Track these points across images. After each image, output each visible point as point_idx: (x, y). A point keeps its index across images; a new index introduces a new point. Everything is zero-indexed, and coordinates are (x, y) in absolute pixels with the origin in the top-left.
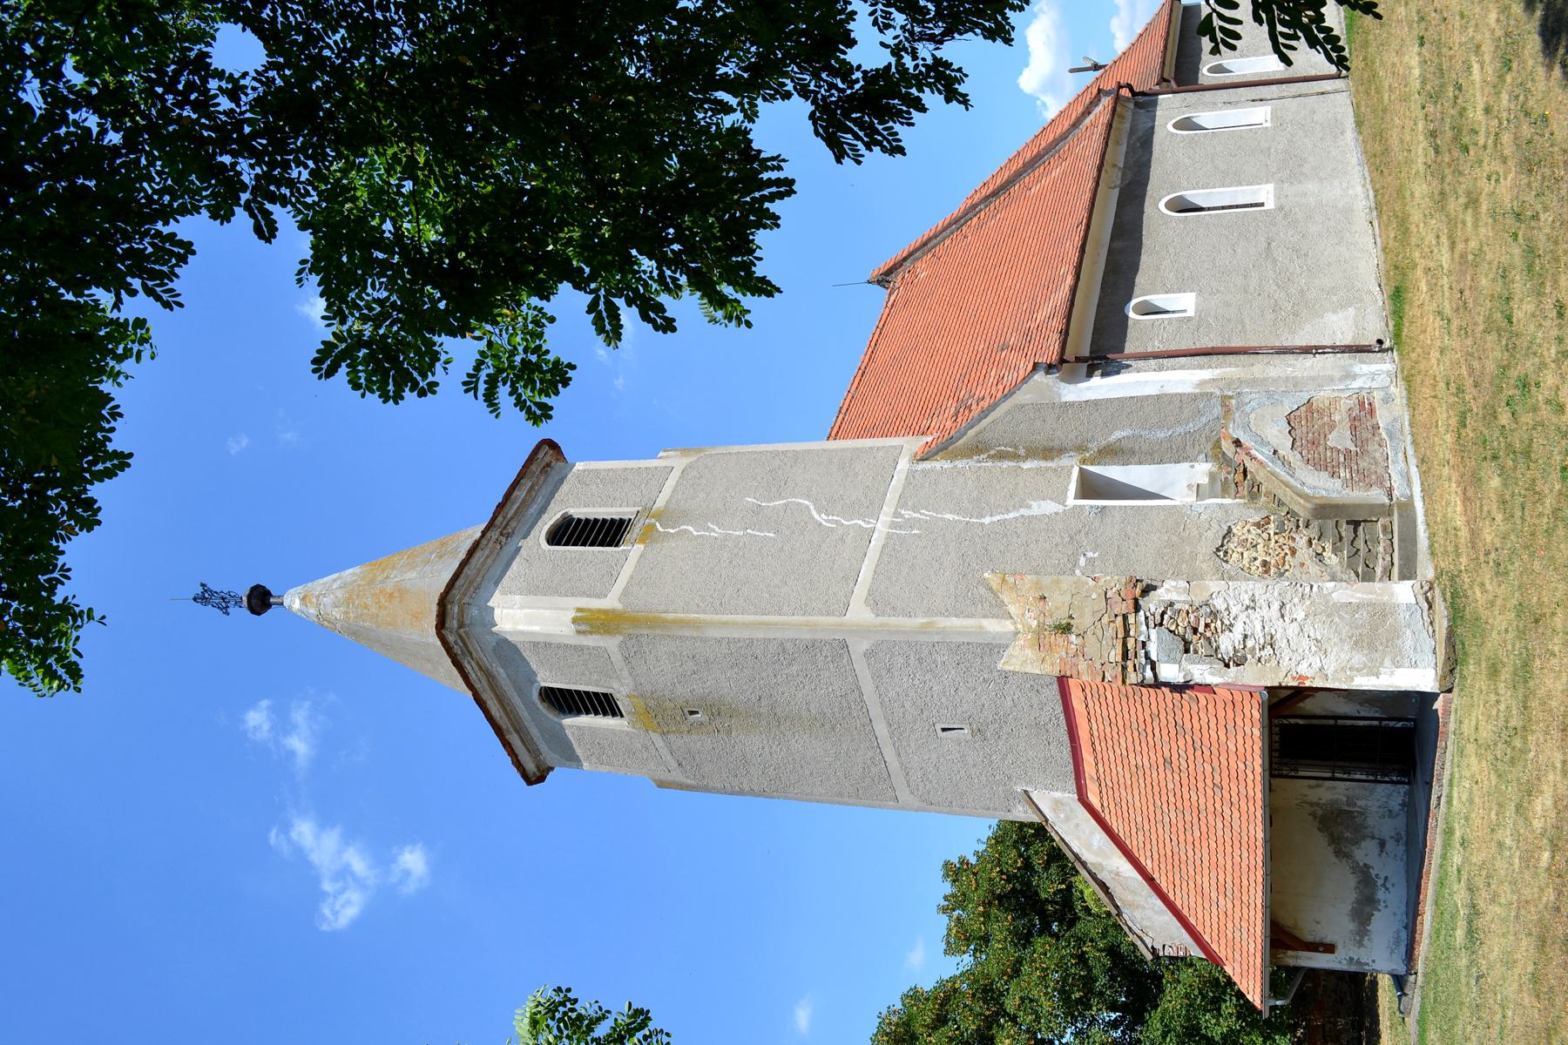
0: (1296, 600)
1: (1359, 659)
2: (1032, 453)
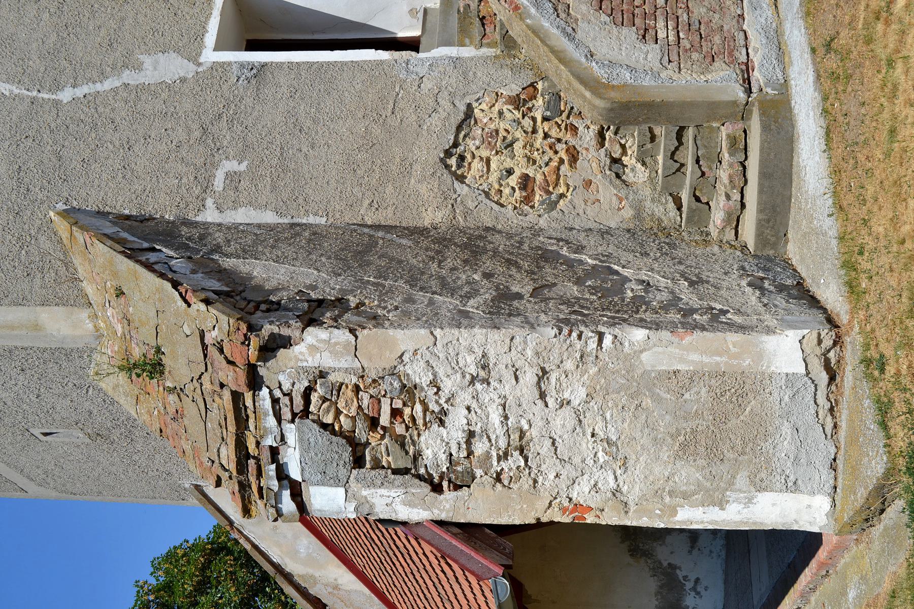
0: (569, 365)
1: (687, 474)
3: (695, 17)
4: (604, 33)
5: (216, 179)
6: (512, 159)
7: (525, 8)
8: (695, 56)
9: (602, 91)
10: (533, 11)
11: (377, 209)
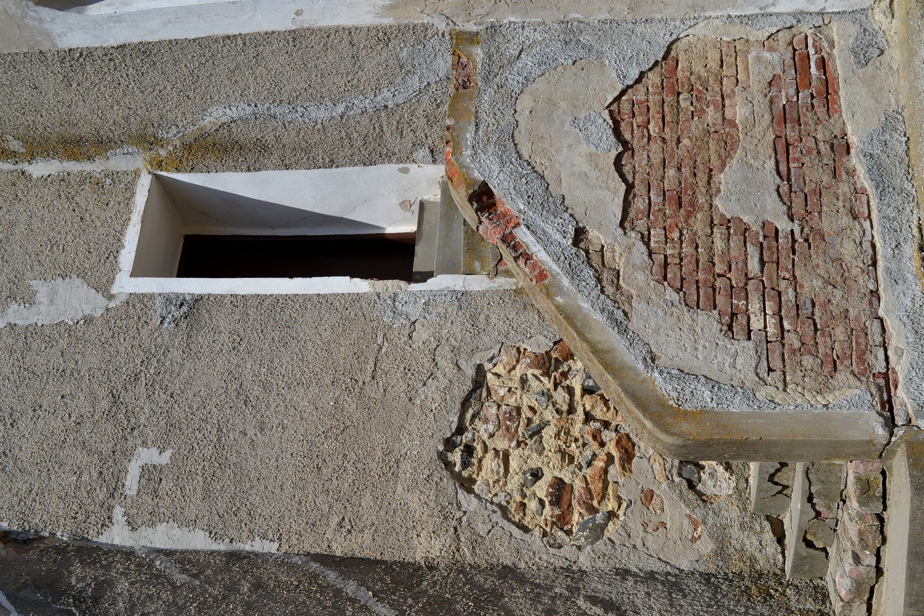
2: (38, 148)
3: (805, 300)
4: (671, 321)
5: (129, 477)
6: (540, 454)
7: (554, 277)
8: (808, 361)
9: (669, 420)
10: (565, 281)
11: (349, 532)
